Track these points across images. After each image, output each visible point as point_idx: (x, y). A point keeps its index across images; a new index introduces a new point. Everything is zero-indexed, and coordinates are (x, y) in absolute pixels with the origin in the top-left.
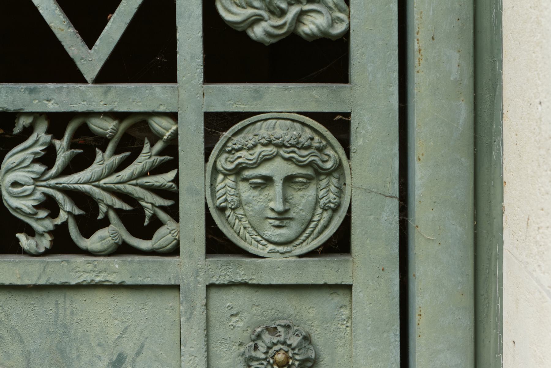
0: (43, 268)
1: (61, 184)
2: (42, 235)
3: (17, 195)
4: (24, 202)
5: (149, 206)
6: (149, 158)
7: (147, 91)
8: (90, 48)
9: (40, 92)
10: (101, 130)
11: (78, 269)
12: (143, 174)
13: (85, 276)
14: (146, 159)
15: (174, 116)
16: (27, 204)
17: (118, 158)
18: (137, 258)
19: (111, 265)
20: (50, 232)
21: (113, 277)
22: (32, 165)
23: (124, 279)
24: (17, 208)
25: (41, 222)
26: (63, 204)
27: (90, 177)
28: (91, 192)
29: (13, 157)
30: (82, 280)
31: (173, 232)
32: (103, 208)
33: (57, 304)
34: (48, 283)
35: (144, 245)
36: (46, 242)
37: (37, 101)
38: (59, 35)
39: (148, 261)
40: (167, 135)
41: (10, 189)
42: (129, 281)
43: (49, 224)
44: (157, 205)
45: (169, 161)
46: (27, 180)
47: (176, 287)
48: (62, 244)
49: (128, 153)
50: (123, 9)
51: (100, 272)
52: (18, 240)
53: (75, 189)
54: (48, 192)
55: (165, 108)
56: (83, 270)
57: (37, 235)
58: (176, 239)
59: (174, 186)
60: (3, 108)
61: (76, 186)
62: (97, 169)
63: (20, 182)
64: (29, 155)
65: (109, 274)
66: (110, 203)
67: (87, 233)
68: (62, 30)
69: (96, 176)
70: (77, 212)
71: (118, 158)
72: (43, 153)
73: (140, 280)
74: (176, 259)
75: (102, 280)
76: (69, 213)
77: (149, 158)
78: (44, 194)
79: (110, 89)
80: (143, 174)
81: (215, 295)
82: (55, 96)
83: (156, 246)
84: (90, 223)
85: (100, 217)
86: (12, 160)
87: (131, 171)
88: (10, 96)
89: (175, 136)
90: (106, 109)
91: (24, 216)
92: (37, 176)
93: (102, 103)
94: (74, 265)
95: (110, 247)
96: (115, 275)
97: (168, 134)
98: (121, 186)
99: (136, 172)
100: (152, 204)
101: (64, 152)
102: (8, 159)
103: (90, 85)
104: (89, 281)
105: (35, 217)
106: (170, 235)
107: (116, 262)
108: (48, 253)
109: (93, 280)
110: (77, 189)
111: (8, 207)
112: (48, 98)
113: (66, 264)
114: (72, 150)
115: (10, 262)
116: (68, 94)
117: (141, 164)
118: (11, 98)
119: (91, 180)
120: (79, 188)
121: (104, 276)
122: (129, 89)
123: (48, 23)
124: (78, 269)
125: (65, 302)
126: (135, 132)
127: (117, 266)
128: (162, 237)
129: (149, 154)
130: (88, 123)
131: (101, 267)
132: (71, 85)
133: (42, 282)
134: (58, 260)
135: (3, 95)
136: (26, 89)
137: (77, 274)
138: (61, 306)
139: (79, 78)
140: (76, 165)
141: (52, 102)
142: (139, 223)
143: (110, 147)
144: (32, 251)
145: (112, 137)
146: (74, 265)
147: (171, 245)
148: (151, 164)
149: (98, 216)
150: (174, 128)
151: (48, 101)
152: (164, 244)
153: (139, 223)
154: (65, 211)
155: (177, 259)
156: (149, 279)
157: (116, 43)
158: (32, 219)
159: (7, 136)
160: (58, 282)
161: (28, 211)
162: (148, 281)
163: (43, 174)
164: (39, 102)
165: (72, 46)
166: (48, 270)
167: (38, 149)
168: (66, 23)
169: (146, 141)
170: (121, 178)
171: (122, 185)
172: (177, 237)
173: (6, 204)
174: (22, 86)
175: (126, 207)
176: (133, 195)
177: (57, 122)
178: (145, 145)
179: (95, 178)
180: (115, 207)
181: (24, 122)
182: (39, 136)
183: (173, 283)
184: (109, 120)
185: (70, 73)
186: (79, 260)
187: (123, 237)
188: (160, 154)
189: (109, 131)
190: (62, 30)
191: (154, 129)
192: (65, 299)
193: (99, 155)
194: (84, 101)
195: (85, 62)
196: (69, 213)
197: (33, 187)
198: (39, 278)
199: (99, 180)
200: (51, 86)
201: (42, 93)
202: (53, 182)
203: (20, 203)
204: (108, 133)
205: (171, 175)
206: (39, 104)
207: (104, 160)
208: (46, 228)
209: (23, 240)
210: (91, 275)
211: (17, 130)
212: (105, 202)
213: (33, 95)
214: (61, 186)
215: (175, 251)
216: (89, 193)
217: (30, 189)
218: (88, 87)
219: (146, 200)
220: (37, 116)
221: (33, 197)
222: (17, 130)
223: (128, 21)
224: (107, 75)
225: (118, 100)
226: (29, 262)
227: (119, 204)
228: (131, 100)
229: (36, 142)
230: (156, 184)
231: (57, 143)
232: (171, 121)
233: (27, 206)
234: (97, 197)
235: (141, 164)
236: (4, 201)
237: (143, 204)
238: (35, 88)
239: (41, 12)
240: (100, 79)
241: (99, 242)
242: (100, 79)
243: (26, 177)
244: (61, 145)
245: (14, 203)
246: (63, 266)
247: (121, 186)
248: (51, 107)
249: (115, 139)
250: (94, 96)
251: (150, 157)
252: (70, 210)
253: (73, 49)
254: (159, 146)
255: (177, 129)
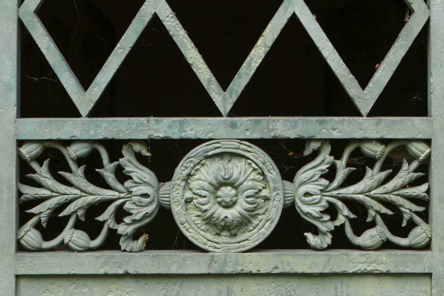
0: (327, 260)
1: (341, 194)
2: (325, 234)
3: (308, 203)
4: (313, 208)
5: (408, 211)
6: (408, 174)
7: (409, 123)
8: (363, 90)
9: (328, 123)
10: (372, 153)
11: (354, 261)
12: (404, 187)
13: (360, 266)
14: (405, 175)
15: (428, 142)
16: (315, 210)
17: (384, 174)
18: (399, 252)
19: (380, 257)
20: (331, 232)
21: (381, 267)
22: (320, 180)
23: (390, 269)
24: (308, 213)
25: (325, 224)
26: (342, 209)
27: (363, 188)
28: (364, 201)
29: (305, 174)
30: (357, 270)
31: (426, 232)
32: (372, 213)
33: (336, 288)
34: (331, 272)
35: (403, 242)
36: (328, 240)
37: (325, 130)
38: (342, 80)
39: (408, 254)
40: (422, 157)
41: (303, 198)
42: (393, 270)
43: (331, 226)
44: (414, 210)
45: (423, 176)
46: (316, 191)
47: (429, 275)
48: (340, 241)
49: (391, 171)
50: (390, 60)
51: (371, 263)
52: (305, 238)
53: (352, 198)
54: (331, 201)
55: (422, 135)
56: (358, 261)
57: (320, 234)
58: (429, 237)
59: (427, 195)
60: (299, 136)
61: (353, 196)
62: (369, 183)
63: (310, 193)
64: (317, 172)
65: (378, 264)
66: (378, 209)
67: (358, 232)
68: (345, 76)
69: (368, 188)
70: (352, 216)
71: (384, 174)
72: (328, 170)
73: (402, 269)
74: (429, 252)
75: (372, 269)
76: (347, 217)
77: (408, 174)
78: (328, 202)
79: (381, 121)
80: (404, 187)
81: (23, 283)
82: (339, 127)
83: (413, 242)
84: (361, 225)
85: (369, 220)
86: (304, 175)
87: (394, 184)
88: (305, 126)
89: (428, 157)
90: (378, 136)
91: (313, 219)
92: (323, 188)
93: (374, 132)
94: (351, 258)
95: (378, 243)
96: (382, 265)
97: (423, 156)
98: (387, 196)
99: (399, 185)
100: (410, 210)
101: (343, 169)
102: (301, 175)
103: (365, 118)
104: (363, 270)
105: (320, 220)
106: (424, 234)
107: (383, 255)
108: (329, 247)
109: (365, 269)
110: (353, 198)
111: (300, 212)
112: (333, 128)
113: (345, 257)
114: (349, 168)
115: (302, 255)
116: (349, 125)
117: (402, 179)
118: (305, 128)
119: (364, 191)
120: (355, 197)
121: (374, 266)
122: (395, 121)
123: (334, 71)
124: (354, 261)
125: (342, 287)
126: (397, 153)
127: (384, 258)
128: (418, 235)
129: (408, 171)
130: (362, 147)
131: (372, 259)
132: (351, 118)
133: (327, 271)
134: (339, 253)
135: (300, 126)
136: (317, 121)
137: (354, 264)
138: (339, 290)
139: (356, 112)
140: (350, 180)
141: (336, 131)
142: (397, 224)
143: (378, 166)
144: (318, 247)
145: (380, 158)
146: (351, 258)
147: (425, 242)
148: (409, 179)
149: (366, 219)
150: (428, 151)
151: (333, 130)
152: (420, 241)
153: (397, 224)
154: (343, 215)
155: (430, 253)
156: (409, 268)
157: (385, 86)
158: (319, 222)
159: (295, 157)
160: (338, 271)
161: (316, 215)
162: (408, 270)
163: (327, 187)
164: (327, 130)
165: (352, 88)
166: (331, 261)
167: (324, 167)
168: (347, 71)
169: (405, 161)
170: (387, 190)
171: (387, 195)
172: (430, 236)
173: (298, 210)
174: (314, 119)
175: (390, 212)
176: (395, 202)
177: (337, 146)
178: (404, 165)
179: (367, 190)
180: (381, 212)
181: (314, 146)
182: (325, 157)
183: (427, 272)
184: (379, 145)
185: (349, 109)
186: (355, 254)
187: (387, 236)
188: (415, 171)
189: (378, 153)
190: (345, 76)
191: (412, 152)
192: (342, 284)
193: (369, 172)
194: (361, 130)
195: (362, 100)
196: (347, 217)
197: (319, 196)
198: (324, 268)
199: (370, 191)
200: (336, 119)
201: (329, 124)
202: (335, 193)
203: (310, 209)
204: (377, 155)
205: (424, 187)
206: (327, 132)
207: (373, 176)
208: (329, 228)
209: (310, 238)
210: (364, 265)
211: (307, 152)
212: (374, 208)
213: (322, 126)
214: (341, 196)
215: (427, 247)
216: (362, 201)
217: (318, 198)
218: (364, 119)
219: (405, 207)
220: (324, 141)
221: (320, 205)
222: (307, 152)
223: (394, 70)
224: (378, 110)
225: (387, 129)
226: (317, 255)
227: (384, 210)
228: (396, 129)
229: (323, 161)
230: (413, 194)
231: (338, 163)
232: (426, 146)
233: (316, 212)
234: (368, 205)
235: (402, 179)
236: (297, 208)
237: (403, 209)
238: (323, 120)
239: (329, 62)
240: (373, 113)
241: (370, 239)
242: (373, 113)
243: (316, 189)
244: (341, 164)
245: (306, 209)
246: (342, 258)
247: (387, 196)
248: (336, 135)
249: (382, 160)
250: (369, 126)
251: (409, 173)
252: (347, 215)
253: (352, 90)
254: (415, 164)
255: (430, 152)
